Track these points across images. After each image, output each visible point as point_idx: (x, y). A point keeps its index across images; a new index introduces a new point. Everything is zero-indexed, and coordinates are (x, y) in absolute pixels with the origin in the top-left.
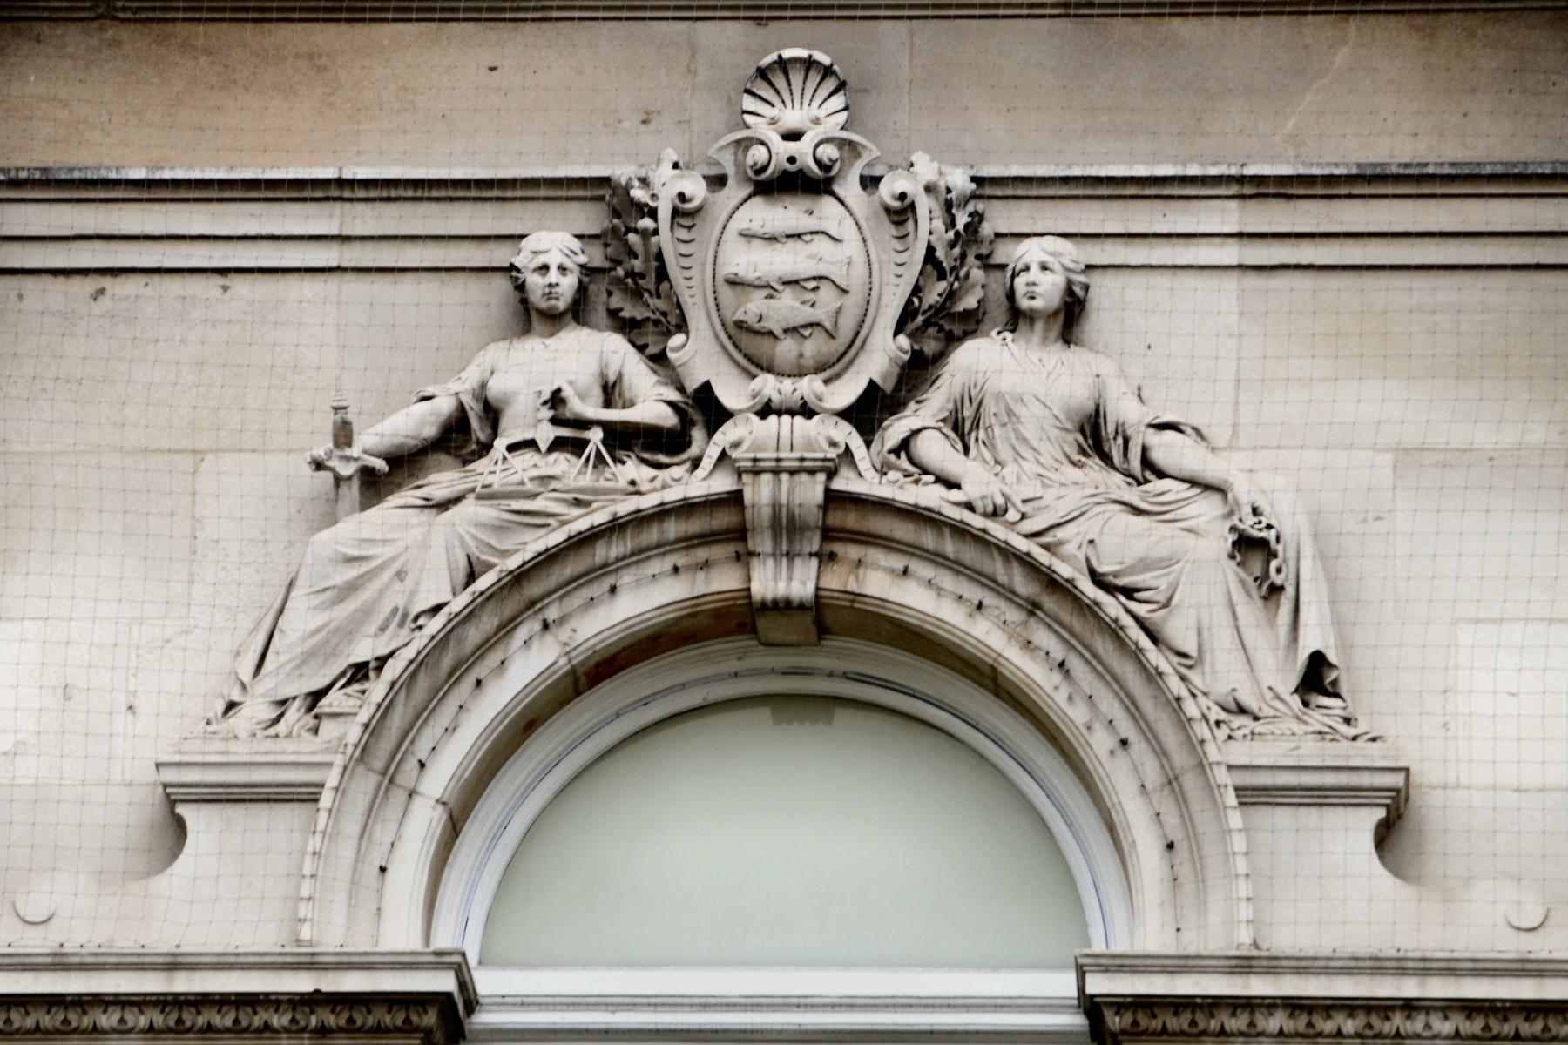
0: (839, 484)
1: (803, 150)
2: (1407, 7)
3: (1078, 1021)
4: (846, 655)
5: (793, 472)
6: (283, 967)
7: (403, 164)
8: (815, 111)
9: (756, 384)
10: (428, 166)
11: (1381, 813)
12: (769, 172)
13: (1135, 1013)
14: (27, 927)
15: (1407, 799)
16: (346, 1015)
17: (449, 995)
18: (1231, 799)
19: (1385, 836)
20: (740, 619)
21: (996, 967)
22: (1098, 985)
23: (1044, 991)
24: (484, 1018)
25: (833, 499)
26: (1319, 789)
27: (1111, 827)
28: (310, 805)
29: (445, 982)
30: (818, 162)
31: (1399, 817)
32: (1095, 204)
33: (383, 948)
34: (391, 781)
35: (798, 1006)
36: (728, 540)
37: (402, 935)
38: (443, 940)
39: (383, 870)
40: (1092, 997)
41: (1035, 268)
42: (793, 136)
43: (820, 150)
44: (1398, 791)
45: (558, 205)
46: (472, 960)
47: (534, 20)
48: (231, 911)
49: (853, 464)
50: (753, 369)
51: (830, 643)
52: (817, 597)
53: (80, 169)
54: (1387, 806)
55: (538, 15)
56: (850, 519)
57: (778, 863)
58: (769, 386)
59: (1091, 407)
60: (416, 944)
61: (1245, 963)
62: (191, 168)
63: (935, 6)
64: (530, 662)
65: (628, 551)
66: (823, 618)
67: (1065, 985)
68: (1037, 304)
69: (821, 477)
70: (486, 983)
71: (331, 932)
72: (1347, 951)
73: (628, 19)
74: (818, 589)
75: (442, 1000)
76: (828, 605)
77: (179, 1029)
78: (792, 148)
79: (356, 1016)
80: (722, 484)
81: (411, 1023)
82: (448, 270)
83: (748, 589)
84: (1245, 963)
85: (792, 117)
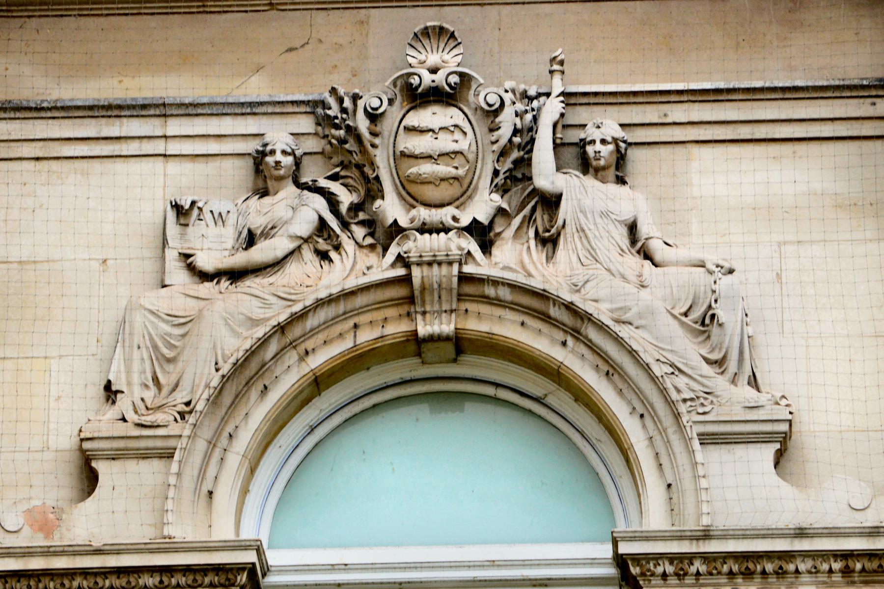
0: (468, 269)
1: (440, 77)
2: (182, 4)
3: (611, 571)
4: (472, 366)
5: (430, 264)
6: (152, 551)
7: (599, 83)
8: (447, 57)
9: (414, 212)
10: (591, 83)
11: (778, 446)
12: (420, 90)
13: (161, 576)
14: (6, 533)
15: (790, 437)
16: (158, 579)
17: (254, 564)
18: (696, 443)
19: (779, 457)
20: (416, 345)
21: (547, 541)
22: (625, 548)
23: (591, 555)
24: (272, 579)
25: (464, 278)
26: (713, 434)
27: (627, 460)
28: (168, 460)
29: (250, 557)
30: (449, 85)
31: (786, 450)
32: (93, 121)
33: (644, 529)
34: (214, 445)
35: (416, 568)
36: (397, 305)
37: (224, 531)
38: (247, 534)
39: (211, 493)
40: (622, 555)
41: (598, 142)
42: (434, 71)
43: (451, 77)
44: (785, 433)
45: (787, 102)
46: (265, 546)
47: (422, 6)
48: (118, 520)
49: (474, 259)
50: (414, 203)
51: (465, 358)
52: (456, 333)
53: (850, 79)
54: (781, 442)
55: (187, 10)
56: (469, 289)
57: (442, 487)
58: (424, 214)
59: (632, 220)
60: (231, 536)
61: (876, 530)
62: (635, 82)
63: (319, 3)
64: (289, 377)
65: (341, 312)
66: (460, 345)
67: (607, 551)
68: (602, 162)
69: (456, 267)
70: (273, 558)
71: (182, 530)
72: (781, 525)
73: (303, 9)
74: (456, 329)
75: (251, 570)
76: (463, 338)
77: (748, 574)
78: (434, 77)
79: (132, 579)
80: (401, 272)
81: (750, 569)
82: (83, 157)
83: (416, 330)
84: (876, 530)
85: (433, 59)
